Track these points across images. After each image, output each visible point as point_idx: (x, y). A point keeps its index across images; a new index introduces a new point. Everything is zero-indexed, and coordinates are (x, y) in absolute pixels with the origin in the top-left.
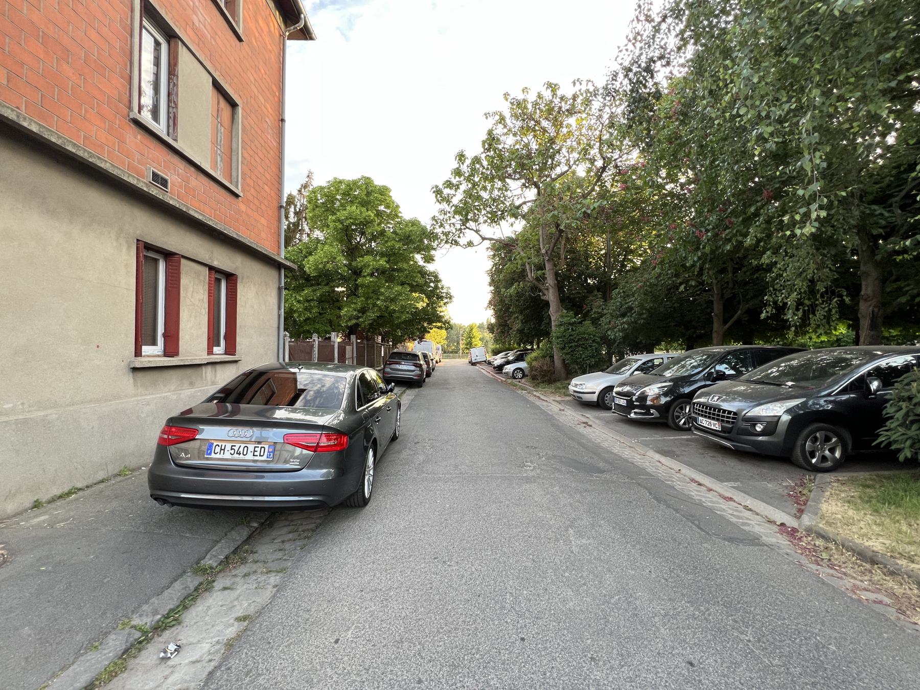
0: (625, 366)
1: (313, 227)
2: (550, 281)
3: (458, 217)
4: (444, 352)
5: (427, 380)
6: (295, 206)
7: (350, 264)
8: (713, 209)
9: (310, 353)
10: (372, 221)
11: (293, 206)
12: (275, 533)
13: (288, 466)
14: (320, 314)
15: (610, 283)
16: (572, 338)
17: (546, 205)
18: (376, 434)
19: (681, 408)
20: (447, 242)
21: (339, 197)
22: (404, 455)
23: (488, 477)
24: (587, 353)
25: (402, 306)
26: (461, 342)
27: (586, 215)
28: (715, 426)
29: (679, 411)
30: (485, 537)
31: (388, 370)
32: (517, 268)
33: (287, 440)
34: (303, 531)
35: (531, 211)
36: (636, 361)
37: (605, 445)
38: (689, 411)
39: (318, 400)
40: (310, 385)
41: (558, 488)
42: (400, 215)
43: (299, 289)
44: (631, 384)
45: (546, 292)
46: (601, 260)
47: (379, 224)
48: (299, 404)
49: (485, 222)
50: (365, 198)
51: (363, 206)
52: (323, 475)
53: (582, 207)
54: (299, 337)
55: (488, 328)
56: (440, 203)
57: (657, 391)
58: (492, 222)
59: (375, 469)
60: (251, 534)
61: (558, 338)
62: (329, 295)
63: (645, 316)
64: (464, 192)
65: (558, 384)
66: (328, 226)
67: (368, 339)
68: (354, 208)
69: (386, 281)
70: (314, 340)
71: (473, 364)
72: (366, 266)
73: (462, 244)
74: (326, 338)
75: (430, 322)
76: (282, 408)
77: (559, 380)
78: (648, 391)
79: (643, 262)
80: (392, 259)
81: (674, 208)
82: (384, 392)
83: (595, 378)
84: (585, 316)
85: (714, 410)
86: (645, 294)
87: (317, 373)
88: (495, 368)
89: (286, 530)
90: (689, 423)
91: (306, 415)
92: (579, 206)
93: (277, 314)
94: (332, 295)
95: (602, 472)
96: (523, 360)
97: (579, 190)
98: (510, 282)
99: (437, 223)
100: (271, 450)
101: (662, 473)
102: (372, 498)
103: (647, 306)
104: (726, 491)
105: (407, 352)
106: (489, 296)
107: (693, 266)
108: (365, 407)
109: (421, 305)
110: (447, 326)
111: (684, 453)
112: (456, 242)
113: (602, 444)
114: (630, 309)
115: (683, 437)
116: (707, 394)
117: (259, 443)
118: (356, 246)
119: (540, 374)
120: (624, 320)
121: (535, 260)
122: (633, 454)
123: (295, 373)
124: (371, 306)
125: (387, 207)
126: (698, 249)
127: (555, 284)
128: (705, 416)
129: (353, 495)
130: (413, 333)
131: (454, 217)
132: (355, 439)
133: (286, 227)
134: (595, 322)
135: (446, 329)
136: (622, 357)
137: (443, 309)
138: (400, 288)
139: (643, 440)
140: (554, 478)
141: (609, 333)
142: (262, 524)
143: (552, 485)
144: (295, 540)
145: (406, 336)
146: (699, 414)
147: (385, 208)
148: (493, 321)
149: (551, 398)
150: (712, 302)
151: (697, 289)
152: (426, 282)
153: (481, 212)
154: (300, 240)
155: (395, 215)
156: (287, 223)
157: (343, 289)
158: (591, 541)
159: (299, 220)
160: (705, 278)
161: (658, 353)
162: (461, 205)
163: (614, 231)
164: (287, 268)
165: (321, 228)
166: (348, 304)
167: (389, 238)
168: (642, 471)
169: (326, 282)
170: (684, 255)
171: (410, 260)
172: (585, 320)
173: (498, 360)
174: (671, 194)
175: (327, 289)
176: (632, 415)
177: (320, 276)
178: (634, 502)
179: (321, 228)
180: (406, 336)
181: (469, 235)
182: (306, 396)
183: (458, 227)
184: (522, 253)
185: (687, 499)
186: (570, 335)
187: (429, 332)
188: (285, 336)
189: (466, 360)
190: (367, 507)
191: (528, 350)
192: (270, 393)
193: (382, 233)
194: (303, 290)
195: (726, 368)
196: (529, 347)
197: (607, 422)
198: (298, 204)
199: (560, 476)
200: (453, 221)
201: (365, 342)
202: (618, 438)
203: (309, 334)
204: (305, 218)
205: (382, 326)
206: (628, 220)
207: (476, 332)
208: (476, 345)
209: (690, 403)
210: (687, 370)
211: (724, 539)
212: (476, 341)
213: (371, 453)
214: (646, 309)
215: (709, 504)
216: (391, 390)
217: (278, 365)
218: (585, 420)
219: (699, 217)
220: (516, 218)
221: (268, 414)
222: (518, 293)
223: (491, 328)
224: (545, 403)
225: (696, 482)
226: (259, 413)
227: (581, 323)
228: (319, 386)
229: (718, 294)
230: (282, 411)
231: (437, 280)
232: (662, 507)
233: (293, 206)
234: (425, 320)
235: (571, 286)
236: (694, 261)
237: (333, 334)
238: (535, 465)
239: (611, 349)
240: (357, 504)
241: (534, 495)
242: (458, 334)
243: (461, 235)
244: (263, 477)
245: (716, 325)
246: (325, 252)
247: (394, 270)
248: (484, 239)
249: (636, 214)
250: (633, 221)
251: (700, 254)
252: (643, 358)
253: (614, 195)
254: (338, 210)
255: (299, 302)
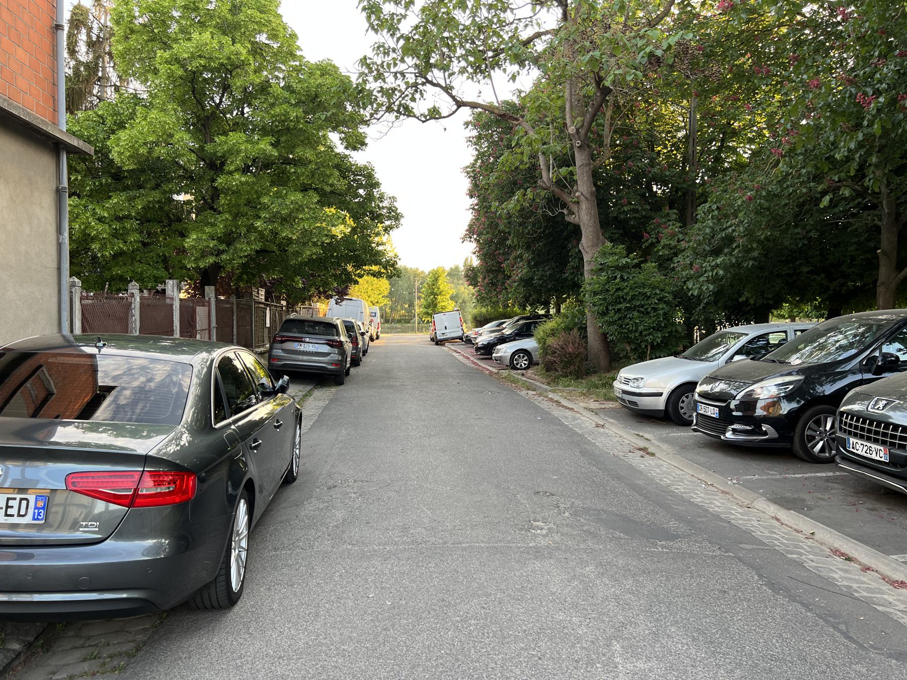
0: (719, 345)
1: (125, 72)
2: (583, 186)
3: (410, 61)
4: (386, 320)
5: (352, 371)
6: (90, 29)
7: (202, 148)
8: (889, 52)
9: (124, 320)
10: (242, 65)
11: (84, 31)
12: (54, 662)
13: (79, 535)
14: (145, 245)
15: (693, 194)
16: (620, 293)
17: (578, 40)
18: (253, 471)
19: (818, 423)
20: (389, 109)
21: (176, 14)
22: (309, 508)
23: (465, 549)
24: (649, 321)
25: (304, 232)
26: (416, 302)
27: (654, 60)
28: (878, 453)
29: (814, 426)
30: (458, 660)
31: (278, 352)
32: (522, 162)
33: (74, 485)
34: (110, 657)
35: (551, 50)
36: (738, 336)
37: (679, 489)
38: (833, 427)
39: (140, 405)
40: (125, 378)
41: (592, 567)
42: (298, 53)
43: (100, 195)
44: (728, 378)
45: (574, 208)
46: (678, 149)
47: (257, 71)
48: (102, 412)
49: (463, 71)
50: (229, 16)
51: (224, 33)
52: (148, 551)
53: (647, 45)
54: (103, 289)
55: (467, 276)
56: (376, 31)
57: (774, 391)
58: (475, 73)
59: (250, 537)
60: (9, 664)
61: (595, 293)
62: (161, 208)
63: (756, 254)
64: (423, 10)
65: (594, 379)
66: (156, 72)
67: (238, 294)
68: (207, 36)
69: (273, 184)
70: (132, 295)
71: (439, 342)
72: (233, 151)
73: (418, 113)
74: (157, 292)
75: (359, 264)
76: (69, 424)
77: (595, 372)
78: (759, 391)
79: (754, 154)
80: (283, 139)
81: (816, 51)
82: (269, 394)
83: (667, 365)
84: (646, 254)
85: (878, 426)
86: (757, 213)
87: (139, 356)
88: (478, 349)
89: (78, 654)
90: (831, 449)
91: (117, 436)
92: (640, 43)
93: (54, 242)
94: (166, 208)
95: (671, 536)
96: (530, 335)
97: (640, 14)
98: (508, 189)
99: (371, 71)
100: (41, 504)
101: (780, 538)
102: (245, 592)
103: (761, 235)
104: (895, 569)
105: (315, 318)
106: (468, 217)
107: (848, 159)
108: (230, 420)
109: (340, 231)
110: (391, 270)
111: (821, 502)
112: (406, 108)
113: (672, 488)
114: (730, 240)
115: (819, 474)
116: (867, 397)
117: (22, 490)
118: (213, 113)
119: (561, 361)
120: (719, 261)
121: (556, 147)
122: (729, 505)
123: (92, 356)
124: (243, 230)
125: (274, 36)
126: (858, 126)
127: (592, 193)
128: (862, 437)
129: (207, 586)
130: (326, 284)
131: (402, 61)
132: (211, 481)
133: (70, 72)
134: (664, 264)
135: (389, 277)
136: (711, 329)
137: (384, 238)
138: (299, 196)
139: (747, 480)
140: (585, 550)
141: (690, 284)
142: (29, 646)
143: (582, 562)
144: (94, 674)
145: (313, 290)
146: (850, 433)
147: (268, 38)
148: (476, 262)
149: (580, 404)
150: (878, 229)
151: (851, 205)
152: (350, 187)
153: (455, 51)
154: (100, 99)
155: (289, 53)
156: (72, 63)
157: (188, 197)
158: (653, 663)
159: (97, 58)
160: (867, 182)
161: (775, 323)
162: (416, 37)
163: (703, 94)
164: (72, 150)
165: (141, 74)
166: (199, 225)
167: (276, 99)
168: (745, 536)
169: (153, 183)
170: (832, 139)
171: (318, 143)
172: (645, 261)
173: (485, 336)
174: (811, 23)
175: (156, 195)
176: (729, 435)
177: (142, 171)
178: (732, 593)
179: (141, 74)
180: (313, 290)
181: (432, 97)
182: (116, 397)
183: (411, 79)
184: (531, 133)
185: (826, 586)
186: (618, 289)
187: (356, 282)
188: (73, 285)
189: (426, 336)
190: (236, 608)
191: (539, 317)
192: (42, 395)
193: (264, 88)
194: (110, 197)
195: (900, 350)
196: (542, 312)
197: (683, 448)
198: (95, 26)
199: (596, 547)
200: (401, 67)
201: (233, 299)
202: (702, 476)
203: (122, 282)
204: (110, 54)
205: (266, 269)
206: (730, 71)
207: (444, 285)
208: (443, 308)
209: (833, 413)
210: (830, 354)
211: (890, 656)
212: (445, 301)
213: (242, 507)
214: (759, 242)
215: (866, 594)
216: (283, 389)
217: (59, 341)
218: (642, 444)
219: (863, 68)
220: (522, 64)
221: (40, 435)
222: (523, 209)
223: (472, 276)
224: (569, 413)
225: (843, 554)
226: (23, 433)
227: (638, 266)
228: (142, 379)
229: (889, 214)
230: (71, 429)
231: (372, 183)
232: (781, 600)
233: (84, 31)
234: (348, 259)
235: (620, 198)
236: (849, 150)
237: (170, 285)
238: (551, 525)
239: (691, 314)
240: (215, 604)
241: (548, 581)
242: (410, 288)
243: (417, 96)
244: (30, 557)
245: (884, 272)
246: (150, 123)
247: (288, 162)
248: (460, 104)
249: (746, 61)
250: (740, 75)
251: (860, 136)
252: (751, 331)
253: (706, 23)
254: (176, 40)
255: (101, 220)
